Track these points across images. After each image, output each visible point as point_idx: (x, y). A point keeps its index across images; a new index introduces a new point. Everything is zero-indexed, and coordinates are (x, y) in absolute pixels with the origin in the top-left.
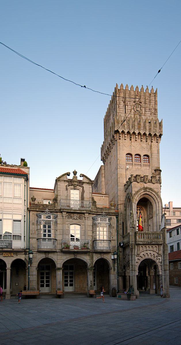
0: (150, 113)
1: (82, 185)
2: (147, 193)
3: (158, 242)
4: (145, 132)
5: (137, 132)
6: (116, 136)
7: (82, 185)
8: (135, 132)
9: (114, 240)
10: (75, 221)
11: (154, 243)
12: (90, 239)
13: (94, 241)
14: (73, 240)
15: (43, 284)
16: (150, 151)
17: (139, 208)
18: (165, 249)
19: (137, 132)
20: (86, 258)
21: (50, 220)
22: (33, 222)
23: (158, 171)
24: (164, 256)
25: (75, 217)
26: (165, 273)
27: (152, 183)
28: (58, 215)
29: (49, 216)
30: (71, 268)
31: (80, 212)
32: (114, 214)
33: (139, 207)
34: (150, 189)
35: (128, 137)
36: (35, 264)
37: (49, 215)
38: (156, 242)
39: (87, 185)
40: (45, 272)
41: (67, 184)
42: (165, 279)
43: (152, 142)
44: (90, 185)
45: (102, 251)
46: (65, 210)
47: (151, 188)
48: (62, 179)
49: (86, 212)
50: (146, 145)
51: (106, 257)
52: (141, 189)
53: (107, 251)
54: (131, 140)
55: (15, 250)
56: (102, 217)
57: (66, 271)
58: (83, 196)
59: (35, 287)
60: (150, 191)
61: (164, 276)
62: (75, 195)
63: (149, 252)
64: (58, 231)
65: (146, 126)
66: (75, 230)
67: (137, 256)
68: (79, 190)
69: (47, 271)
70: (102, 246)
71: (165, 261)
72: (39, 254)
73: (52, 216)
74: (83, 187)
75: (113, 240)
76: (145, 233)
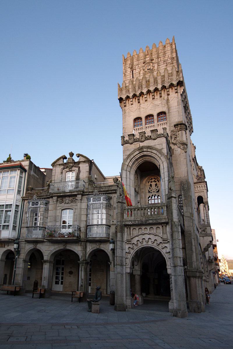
0: (165, 65)
1: (78, 165)
2: (145, 153)
3: (159, 219)
4: (156, 87)
5: (145, 91)
7: (79, 165)
8: (143, 91)
10: (66, 206)
11: (151, 222)
12: (83, 225)
14: (64, 227)
15: (58, 280)
16: (166, 106)
17: (154, 180)
19: (145, 91)
20: (77, 249)
21: (38, 206)
22: (27, 211)
23: (179, 126)
24: (172, 242)
26: (175, 271)
27: (152, 139)
28: (50, 201)
29: (36, 203)
31: (71, 194)
33: (154, 178)
34: (149, 147)
35: (135, 102)
36: (23, 255)
38: (155, 220)
39: (83, 164)
41: (62, 167)
42: (176, 281)
43: (168, 95)
44: (87, 163)
45: (94, 239)
46: (55, 194)
47: (149, 146)
48: (58, 163)
50: (160, 101)
51: (103, 247)
52: (134, 151)
53: (100, 239)
54: (139, 102)
55: (2, 240)
56: (95, 197)
58: (79, 177)
59: (20, 281)
60: (149, 150)
61: (174, 276)
62: (71, 176)
63: (147, 237)
64: (49, 218)
65: (157, 80)
66: (68, 216)
67: (127, 242)
68: (75, 171)
70: (98, 233)
72: (28, 244)
73: (39, 203)
74: (79, 168)
75: (113, 225)
76: (136, 208)
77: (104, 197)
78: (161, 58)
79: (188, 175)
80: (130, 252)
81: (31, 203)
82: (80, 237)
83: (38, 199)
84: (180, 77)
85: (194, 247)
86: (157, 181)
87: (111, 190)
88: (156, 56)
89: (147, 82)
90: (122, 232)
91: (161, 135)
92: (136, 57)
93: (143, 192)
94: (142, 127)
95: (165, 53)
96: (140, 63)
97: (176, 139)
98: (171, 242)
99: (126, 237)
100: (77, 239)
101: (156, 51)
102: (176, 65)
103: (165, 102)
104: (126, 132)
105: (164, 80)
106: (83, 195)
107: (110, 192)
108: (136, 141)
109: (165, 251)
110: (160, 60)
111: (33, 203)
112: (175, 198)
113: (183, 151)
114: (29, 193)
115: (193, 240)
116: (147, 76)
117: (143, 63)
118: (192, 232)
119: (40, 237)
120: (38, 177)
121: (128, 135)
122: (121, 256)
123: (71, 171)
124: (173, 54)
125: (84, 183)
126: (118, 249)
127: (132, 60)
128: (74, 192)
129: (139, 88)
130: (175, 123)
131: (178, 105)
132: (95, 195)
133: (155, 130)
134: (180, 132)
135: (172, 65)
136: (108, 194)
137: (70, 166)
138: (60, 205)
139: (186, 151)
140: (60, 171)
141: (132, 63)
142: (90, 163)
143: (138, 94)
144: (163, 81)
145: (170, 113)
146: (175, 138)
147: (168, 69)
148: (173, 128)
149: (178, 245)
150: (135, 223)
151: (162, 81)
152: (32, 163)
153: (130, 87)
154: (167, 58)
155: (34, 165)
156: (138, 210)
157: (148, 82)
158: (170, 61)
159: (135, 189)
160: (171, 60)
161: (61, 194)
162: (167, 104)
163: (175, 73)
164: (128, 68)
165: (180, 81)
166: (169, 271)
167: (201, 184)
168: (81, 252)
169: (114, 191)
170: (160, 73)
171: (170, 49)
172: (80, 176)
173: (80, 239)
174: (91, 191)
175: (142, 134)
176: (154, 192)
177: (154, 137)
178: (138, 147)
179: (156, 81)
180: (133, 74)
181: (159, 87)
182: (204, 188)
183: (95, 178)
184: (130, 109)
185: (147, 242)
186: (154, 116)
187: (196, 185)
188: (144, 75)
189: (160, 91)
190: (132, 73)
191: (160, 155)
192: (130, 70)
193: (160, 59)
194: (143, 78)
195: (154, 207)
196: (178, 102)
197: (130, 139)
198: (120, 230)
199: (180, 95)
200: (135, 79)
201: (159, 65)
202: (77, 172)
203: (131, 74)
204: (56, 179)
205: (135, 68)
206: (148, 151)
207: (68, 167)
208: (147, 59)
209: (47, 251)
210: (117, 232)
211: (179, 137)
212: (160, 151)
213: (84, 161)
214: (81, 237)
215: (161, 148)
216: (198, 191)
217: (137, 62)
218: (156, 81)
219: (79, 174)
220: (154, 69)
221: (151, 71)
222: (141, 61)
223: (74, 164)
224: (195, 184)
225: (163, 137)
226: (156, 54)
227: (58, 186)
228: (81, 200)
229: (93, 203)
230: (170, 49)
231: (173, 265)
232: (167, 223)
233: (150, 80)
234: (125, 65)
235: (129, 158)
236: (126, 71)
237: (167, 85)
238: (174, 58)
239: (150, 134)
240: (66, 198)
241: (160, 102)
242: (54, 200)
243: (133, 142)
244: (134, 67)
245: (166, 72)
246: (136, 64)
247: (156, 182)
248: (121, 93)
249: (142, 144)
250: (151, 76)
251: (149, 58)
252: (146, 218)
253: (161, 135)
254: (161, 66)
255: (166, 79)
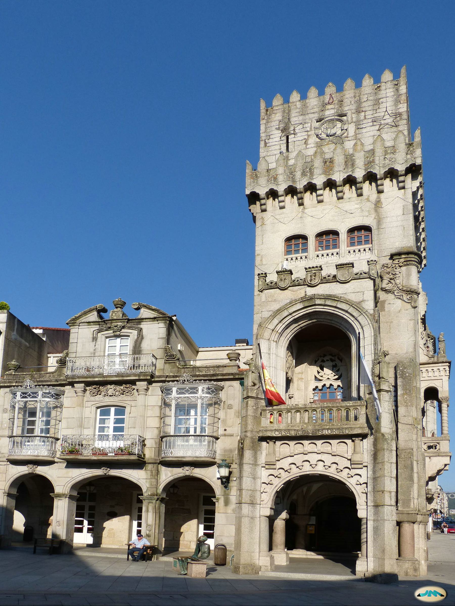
0: (377, 127)
1: (137, 325)
3: (346, 428)
4: (350, 173)
5: (319, 181)
6: (256, 208)
7: (139, 326)
9: (232, 435)
11: (326, 432)
13: (162, 438)
16: (373, 216)
17: (331, 357)
18: (379, 446)
19: (319, 181)
24: (374, 467)
25: (110, 392)
27: (338, 281)
28: (66, 391)
29: (33, 393)
30: (93, 497)
31: (121, 378)
32: (232, 377)
37: (35, 390)
38: (338, 429)
40: (87, 504)
41: (97, 327)
43: (380, 192)
44: (159, 322)
47: (330, 296)
49: (137, 378)
52: (292, 303)
53: (195, 459)
57: (82, 503)
60: (328, 302)
67: (267, 466)
69: (92, 504)
71: (379, 479)
76: (292, 409)
77: (206, 386)
78: (367, 113)
79: (415, 351)
80: (270, 483)
81: (19, 394)
82: (144, 455)
83: (36, 386)
84: (416, 156)
85: (415, 475)
86: (337, 360)
87: (223, 375)
88: (353, 107)
89: (328, 163)
90: (255, 449)
91: (361, 274)
92: (298, 106)
93: (302, 379)
94: (306, 254)
95: (377, 103)
96: (307, 121)
97: (392, 281)
98: (370, 467)
99: (262, 459)
100: (139, 460)
101: (355, 97)
102: (406, 131)
103: (370, 206)
104: (264, 263)
105: (373, 161)
106: (150, 382)
107: (220, 377)
108: (296, 284)
109: (357, 483)
110: (362, 118)
111: (23, 393)
112: (387, 391)
113: (409, 306)
114: (11, 375)
115: (415, 463)
116: (326, 149)
117: (317, 122)
118: (415, 450)
119: (46, 454)
120: (27, 344)
121: (277, 272)
122: (252, 488)
123: (119, 336)
124: (401, 106)
125: (154, 360)
126: (244, 478)
127: (287, 111)
128: (129, 376)
129: (304, 174)
130: (394, 251)
131: (403, 214)
132: (183, 383)
133: (349, 264)
134: (404, 268)
135: (395, 129)
136: (215, 380)
137: (116, 326)
138: (93, 398)
139: (415, 306)
140: (91, 336)
141: (286, 120)
142: (168, 322)
143: (302, 187)
144: (369, 163)
145: (382, 230)
146: (391, 279)
147: (384, 136)
148: (387, 260)
149: (388, 472)
150: (288, 435)
151: (366, 163)
152: (14, 317)
153: (281, 170)
154: (383, 114)
155: (19, 321)
156: (298, 411)
157: (330, 162)
158: (389, 120)
159: (287, 373)
160: (392, 119)
161: (97, 379)
162: (376, 211)
163: (402, 147)
164: (274, 128)
165: (415, 164)
166: (361, 514)
167: (437, 365)
168: (146, 482)
169: (231, 375)
170: (362, 144)
171: (393, 93)
172: (141, 346)
173: (144, 459)
174: (171, 374)
175: (314, 272)
176: (328, 379)
177: (345, 278)
178: (303, 295)
179: (349, 161)
180: (288, 142)
181: (359, 174)
182: (443, 373)
183: (179, 350)
184: (278, 217)
185: (339, 470)
186: (339, 234)
187: (424, 367)
188: (319, 146)
189: (361, 182)
190: (285, 141)
191: (355, 314)
192: (280, 135)
193: (363, 114)
194: (316, 153)
195: (337, 407)
196: (403, 209)
197: (281, 280)
198: (251, 445)
199: (411, 193)
200: (292, 155)
201: (359, 127)
202: (136, 337)
203: (281, 142)
204: (79, 349)
205: (294, 130)
206: (347, 312)
207: (110, 328)
208: (327, 113)
209: (64, 478)
210: (244, 449)
211: (401, 278)
212: (357, 306)
213: (155, 318)
214: (147, 456)
215: (361, 299)
216: (429, 378)
217: (301, 118)
218: (349, 161)
219: (141, 343)
220: (345, 135)
221: (339, 140)
222: (311, 116)
223: (127, 323)
224: (421, 366)
225: (368, 279)
226: (353, 103)
227: (88, 364)
228: (147, 390)
229: (178, 396)
230: (393, 93)
231: (372, 504)
232: (363, 436)
233: (336, 158)
234: (268, 122)
235: (278, 316)
236: (269, 136)
237: (379, 171)
238: (400, 114)
239: (333, 271)
240: (109, 386)
241: (358, 206)
242: (78, 390)
243: (290, 286)
244: (292, 128)
245: (379, 144)
246: (298, 122)
247: (335, 361)
248: (254, 182)
249: (310, 291)
250: (339, 150)
251: (332, 112)
252: (315, 426)
253: (361, 274)
254: (364, 130)
255: (377, 159)
